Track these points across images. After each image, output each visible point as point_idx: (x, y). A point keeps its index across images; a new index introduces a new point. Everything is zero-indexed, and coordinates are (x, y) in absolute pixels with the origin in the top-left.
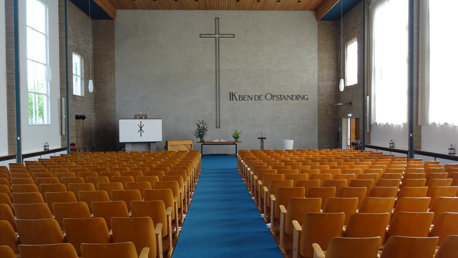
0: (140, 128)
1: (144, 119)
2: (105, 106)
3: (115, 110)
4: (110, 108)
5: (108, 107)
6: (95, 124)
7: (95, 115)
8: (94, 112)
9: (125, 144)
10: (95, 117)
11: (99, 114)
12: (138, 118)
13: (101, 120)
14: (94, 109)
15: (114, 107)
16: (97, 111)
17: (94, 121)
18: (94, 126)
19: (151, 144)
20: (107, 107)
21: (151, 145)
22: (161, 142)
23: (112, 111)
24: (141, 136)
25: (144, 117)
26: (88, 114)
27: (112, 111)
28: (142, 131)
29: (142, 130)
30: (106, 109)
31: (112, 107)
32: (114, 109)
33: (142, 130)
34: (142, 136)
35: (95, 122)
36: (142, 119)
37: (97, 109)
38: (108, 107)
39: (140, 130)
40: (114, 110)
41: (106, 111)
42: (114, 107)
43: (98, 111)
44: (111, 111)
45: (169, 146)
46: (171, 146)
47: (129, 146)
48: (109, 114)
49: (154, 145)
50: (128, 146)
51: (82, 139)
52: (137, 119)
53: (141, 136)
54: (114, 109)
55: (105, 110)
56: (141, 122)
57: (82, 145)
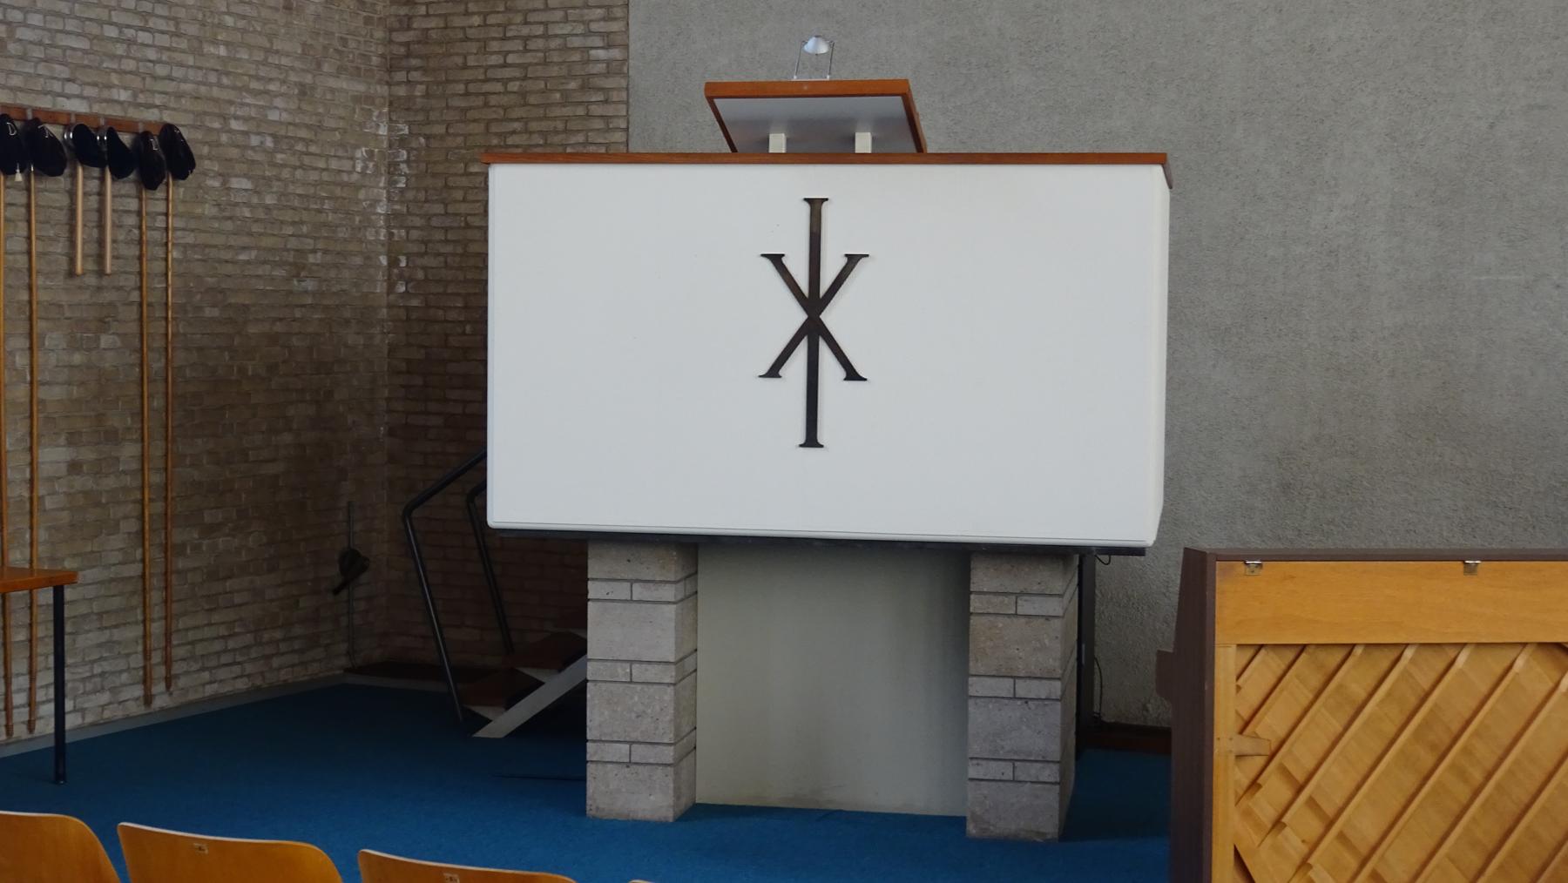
0: (798, 317)
1: (877, 157)
2: (504, 26)
3: (617, 69)
4: (565, 49)
5: (546, 36)
6: (393, 263)
7: (403, 142)
8: (392, 102)
9: (584, 556)
10: (392, 169)
11: (439, 129)
12: (778, 143)
13: (463, 208)
14: (391, 65)
15: (615, 26)
16: (419, 90)
17: (391, 217)
18: (381, 288)
19: (983, 578)
20: (526, 39)
21: (976, 603)
22: (1138, 551)
23: (585, 87)
24: (811, 441)
25: (880, 126)
26: (273, 116)
27: (585, 87)
28: (825, 354)
29: (825, 352)
30: (524, 66)
31: (589, 33)
32: (615, 53)
33: (825, 352)
34: (823, 436)
35: (400, 234)
36: (842, 154)
37: (424, 70)
38: (546, 36)
39: (802, 351)
40: (608, 74)
41: (514, 86)
42: (615, 26)
43: (427, 95)
44: (573, 85)
45: (1226, 660)
46: (1266, 668)
47: (639, 591)
48: (543, 125)
49: (1026, 607)
50: (621, 591)
51: (130, 450)
52: (759, 154)
53: (811, 441)
54: (615, 53)
55: (507, 73)
56: (815, 205)
57: (132, 526)
